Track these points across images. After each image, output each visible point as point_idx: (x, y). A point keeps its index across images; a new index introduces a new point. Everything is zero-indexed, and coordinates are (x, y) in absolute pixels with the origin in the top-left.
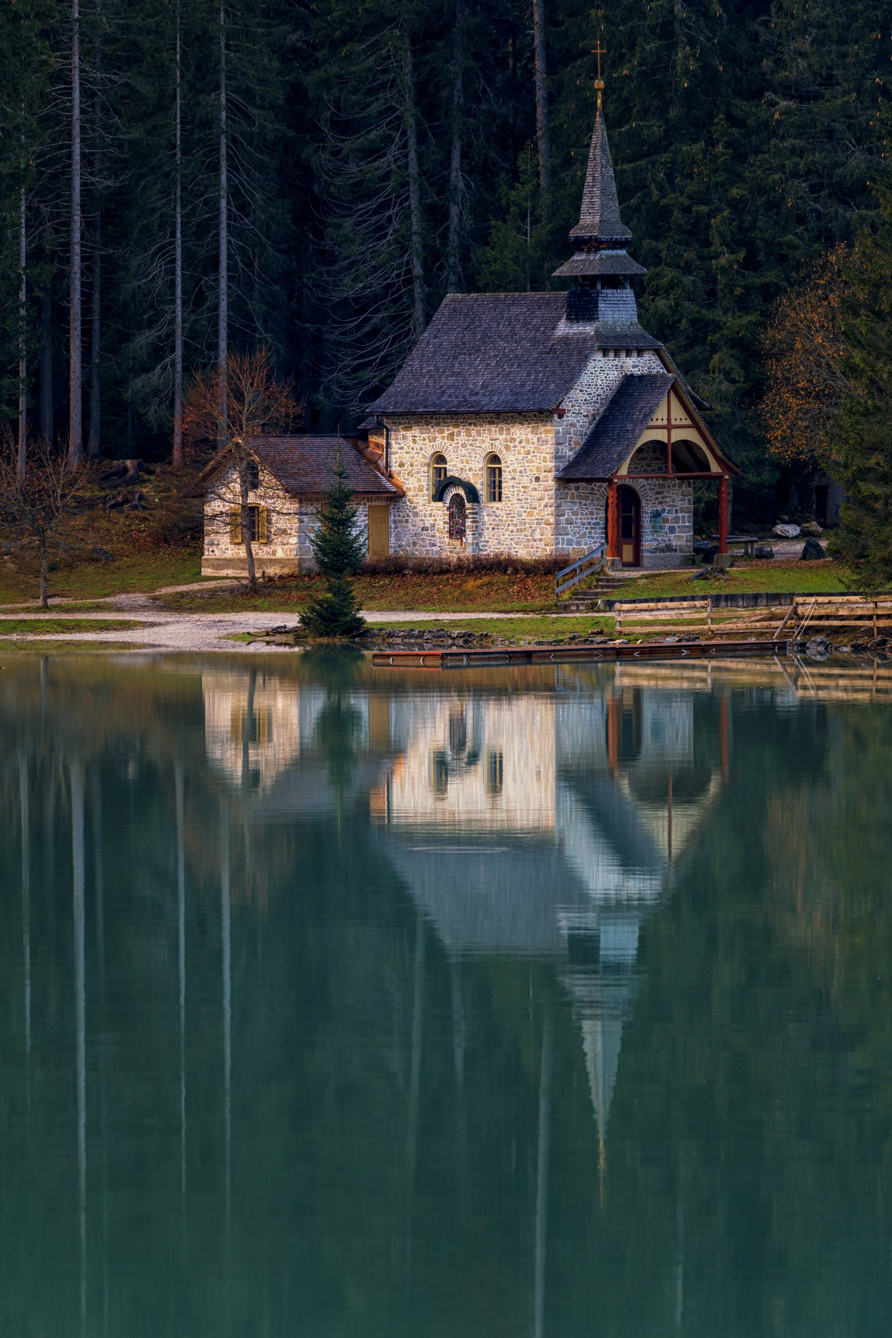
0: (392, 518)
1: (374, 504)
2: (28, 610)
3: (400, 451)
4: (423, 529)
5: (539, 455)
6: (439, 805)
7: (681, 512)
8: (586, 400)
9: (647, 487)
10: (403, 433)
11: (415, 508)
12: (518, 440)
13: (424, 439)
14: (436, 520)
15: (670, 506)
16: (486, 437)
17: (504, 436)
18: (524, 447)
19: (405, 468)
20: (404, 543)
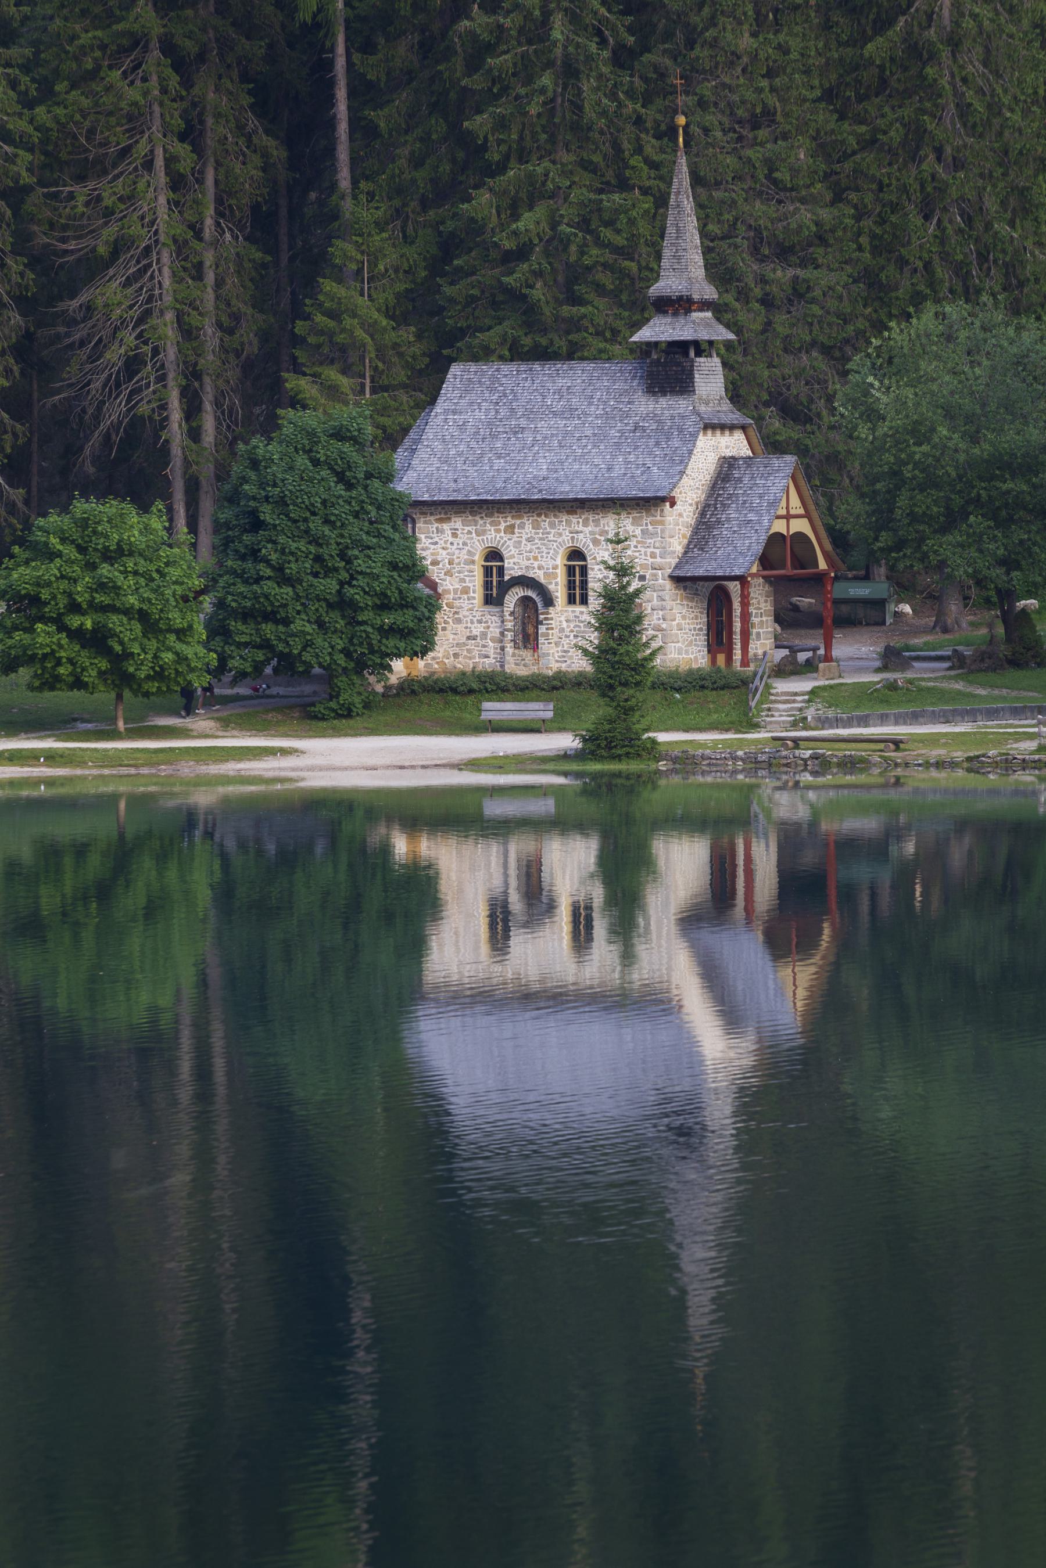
3: (433, 547)
4: (468, 638)
5: (643, 550)
6: (498, 968)
10: (436, 525)
14: (488, 627)
17: (590, 528)
19: (441, 566)
20: (440, 655)
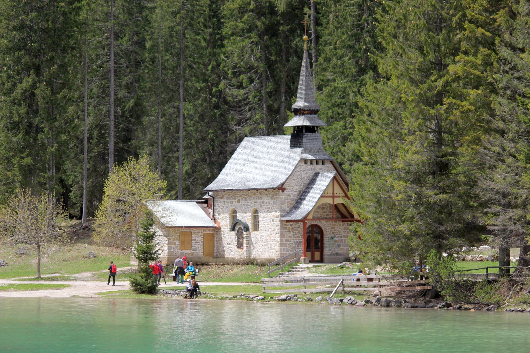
0: (215, 239)
2: (31, 280)
9: (327, 225)
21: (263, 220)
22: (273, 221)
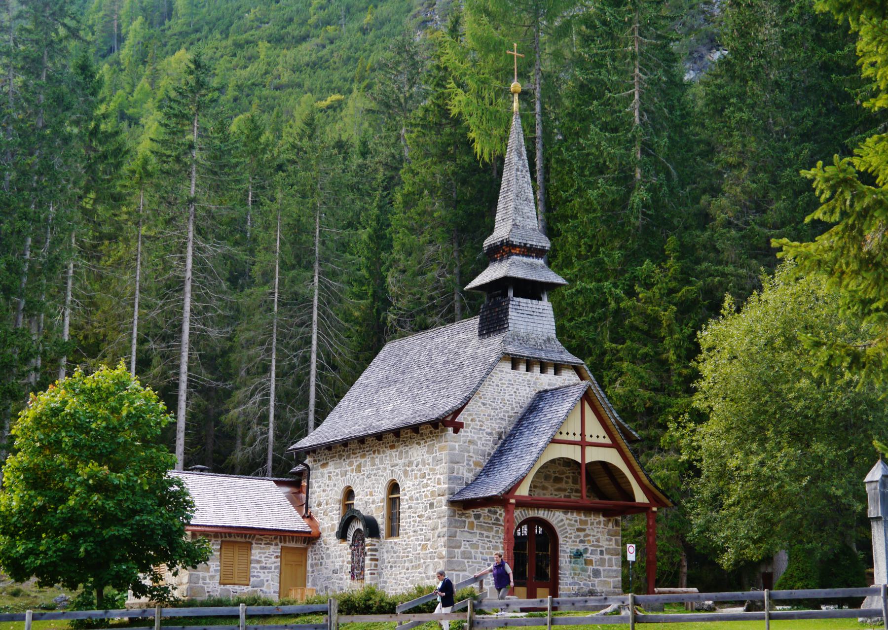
0: (309, 562)
1: (288, 545)
3: (318, 490)
7: (608, 554)
8: (489, 415)
11: (328, 549)
12: (415, 463)
13: (337, 475)
15: (593, 546)
16: (387, 463)
18: (420, 470)
21: (410, 507)
22: (432, 505)
